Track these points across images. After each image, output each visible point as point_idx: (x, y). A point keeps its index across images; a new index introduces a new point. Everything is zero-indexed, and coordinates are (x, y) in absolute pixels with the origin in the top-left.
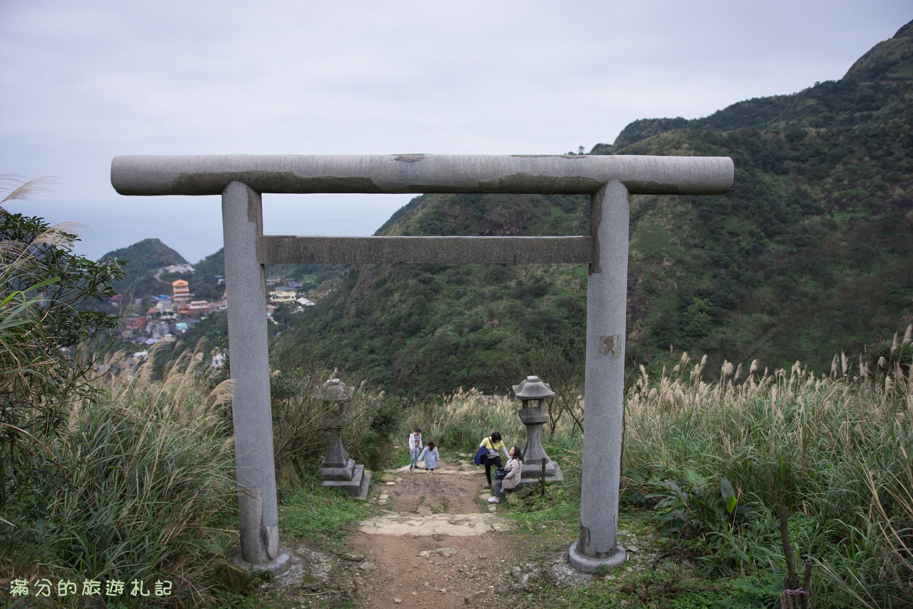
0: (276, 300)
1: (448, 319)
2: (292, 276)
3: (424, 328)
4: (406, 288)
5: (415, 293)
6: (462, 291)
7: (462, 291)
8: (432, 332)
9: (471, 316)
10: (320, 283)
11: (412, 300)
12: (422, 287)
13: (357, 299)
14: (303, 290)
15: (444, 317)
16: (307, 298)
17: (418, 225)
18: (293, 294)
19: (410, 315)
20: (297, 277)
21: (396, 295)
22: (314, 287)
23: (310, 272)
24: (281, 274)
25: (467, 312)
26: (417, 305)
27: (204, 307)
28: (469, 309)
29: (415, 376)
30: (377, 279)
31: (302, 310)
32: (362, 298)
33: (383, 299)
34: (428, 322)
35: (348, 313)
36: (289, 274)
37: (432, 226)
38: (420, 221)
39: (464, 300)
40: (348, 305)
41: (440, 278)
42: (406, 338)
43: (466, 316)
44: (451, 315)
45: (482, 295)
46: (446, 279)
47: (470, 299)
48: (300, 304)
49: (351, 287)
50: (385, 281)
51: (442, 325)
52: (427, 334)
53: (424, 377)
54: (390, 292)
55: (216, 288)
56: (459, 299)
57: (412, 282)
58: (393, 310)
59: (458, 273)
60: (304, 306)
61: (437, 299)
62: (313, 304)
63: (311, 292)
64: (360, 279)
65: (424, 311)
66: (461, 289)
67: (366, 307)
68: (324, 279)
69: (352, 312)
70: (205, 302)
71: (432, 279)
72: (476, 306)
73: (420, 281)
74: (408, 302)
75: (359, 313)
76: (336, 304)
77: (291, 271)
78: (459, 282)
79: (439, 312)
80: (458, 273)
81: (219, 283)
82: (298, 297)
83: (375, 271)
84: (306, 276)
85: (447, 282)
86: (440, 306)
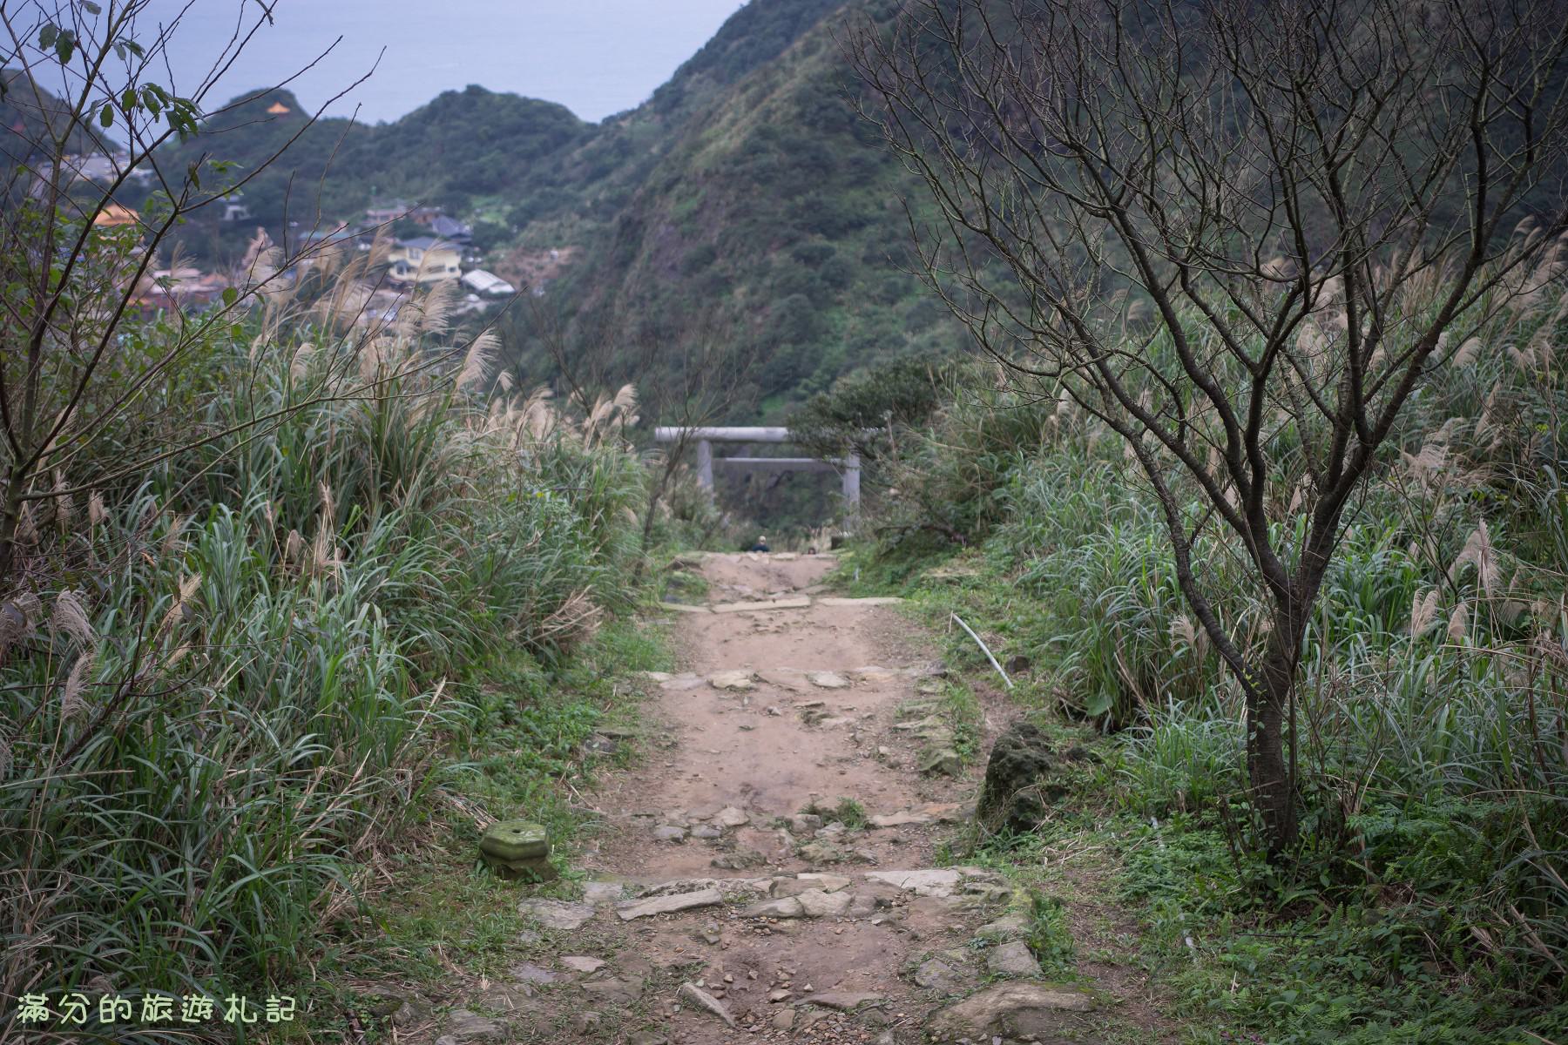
0: (405, 277)
1: (864, 353)
2: (437, 201)
3: (808, 376)
4: (762, 274)
5: (786, 288)
6: (901, 282)
7: (901, 282)
8: (826, 386)
9: (917, 348)
10: (522, 225)
11: (778, 305)
12: (802, 271)
13: (642, 298)
14: (477, 246)
15: (853, 351)
16: (491, 271)
17: (795, 110)
18: (453, 261)
19: (775, 342)
20: (454, 201)
21: (740, 291)
22: (505, 237)
23: (489, 189)
24: (406, 193)
25: (912, 339)
26: (790, 319)
27: (195, 287)
28: (917, 329)
29: (784, 491)
30: (690, 250)
31: (481, 306)
32: (655, 297)
33: (706, 302)
34: (815, 362)
35: (620, 333)
36: (429, 193)
37: (831, 113)
38: (801, 99)
39: (906, 305)
40: (617, 311)
41: (848, 250)
42: (763, 399)
43: (908, 348)
44: (871, 343)
45: (949, 295)
46: (863, 251)
47: (921, 306)
48: (471, 289)
49: (624, 264)
50: (711, 255)
51: (848, 370)
52: (814, 391)
53: (806, 493)
54: (723, 284)
55: (223, 232)
56: (893, 302)
57: (778, 258)
58: (730, 328)
59: (893, 236)
60: (484, 295)
61: (840, 303)
62: (508, 288)
63: (502, 252)
64: (647, 249)
65: (806, 332)
66: (898, 277)
67: (665, 319)
68: (531, 213)
69: (631, 327)
70: (194, 272)
71: (826, 253)
72: (932, 322)
73: (798, 256)
74: (768, 310)
75: (652, 335)
76: (586, 307)
77: (435, 187)
78: (897, 260)
79: (845, 335)
80: (893, 236)
81: (229, 216)
82: (465, 269)
83: (686, 226)
84: (478, 202)
85: (867, 260)
86: (847, 321)
